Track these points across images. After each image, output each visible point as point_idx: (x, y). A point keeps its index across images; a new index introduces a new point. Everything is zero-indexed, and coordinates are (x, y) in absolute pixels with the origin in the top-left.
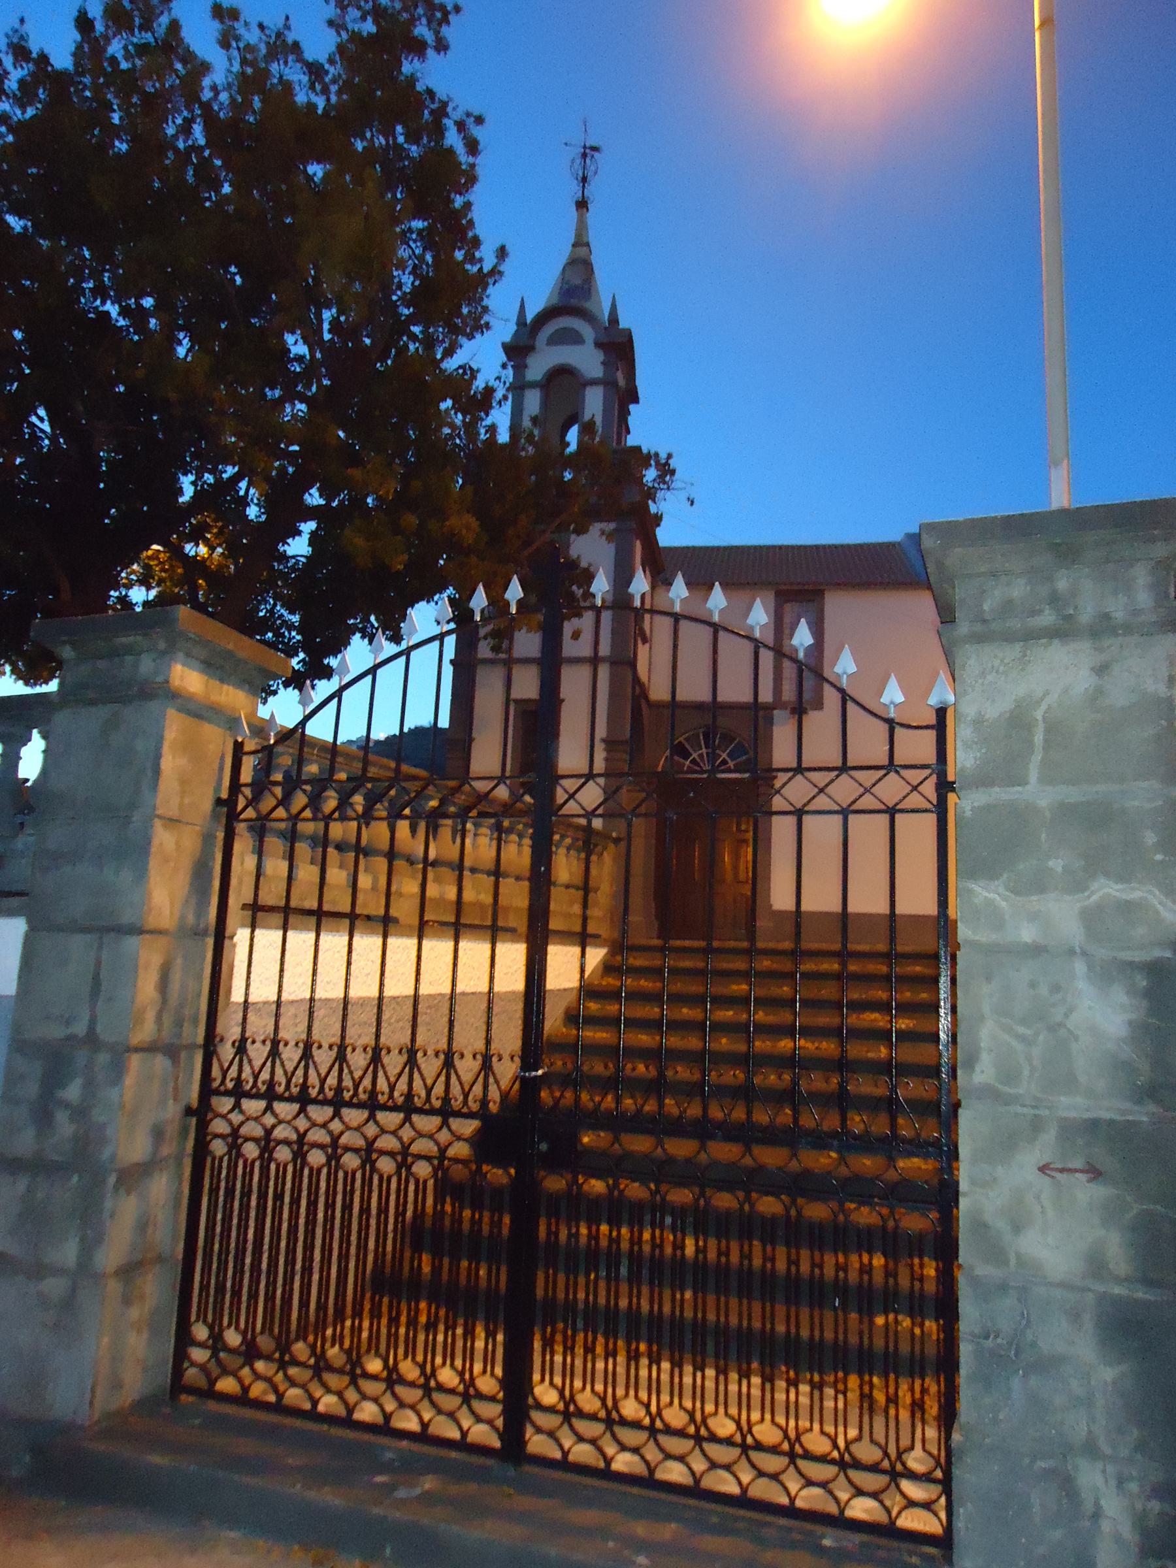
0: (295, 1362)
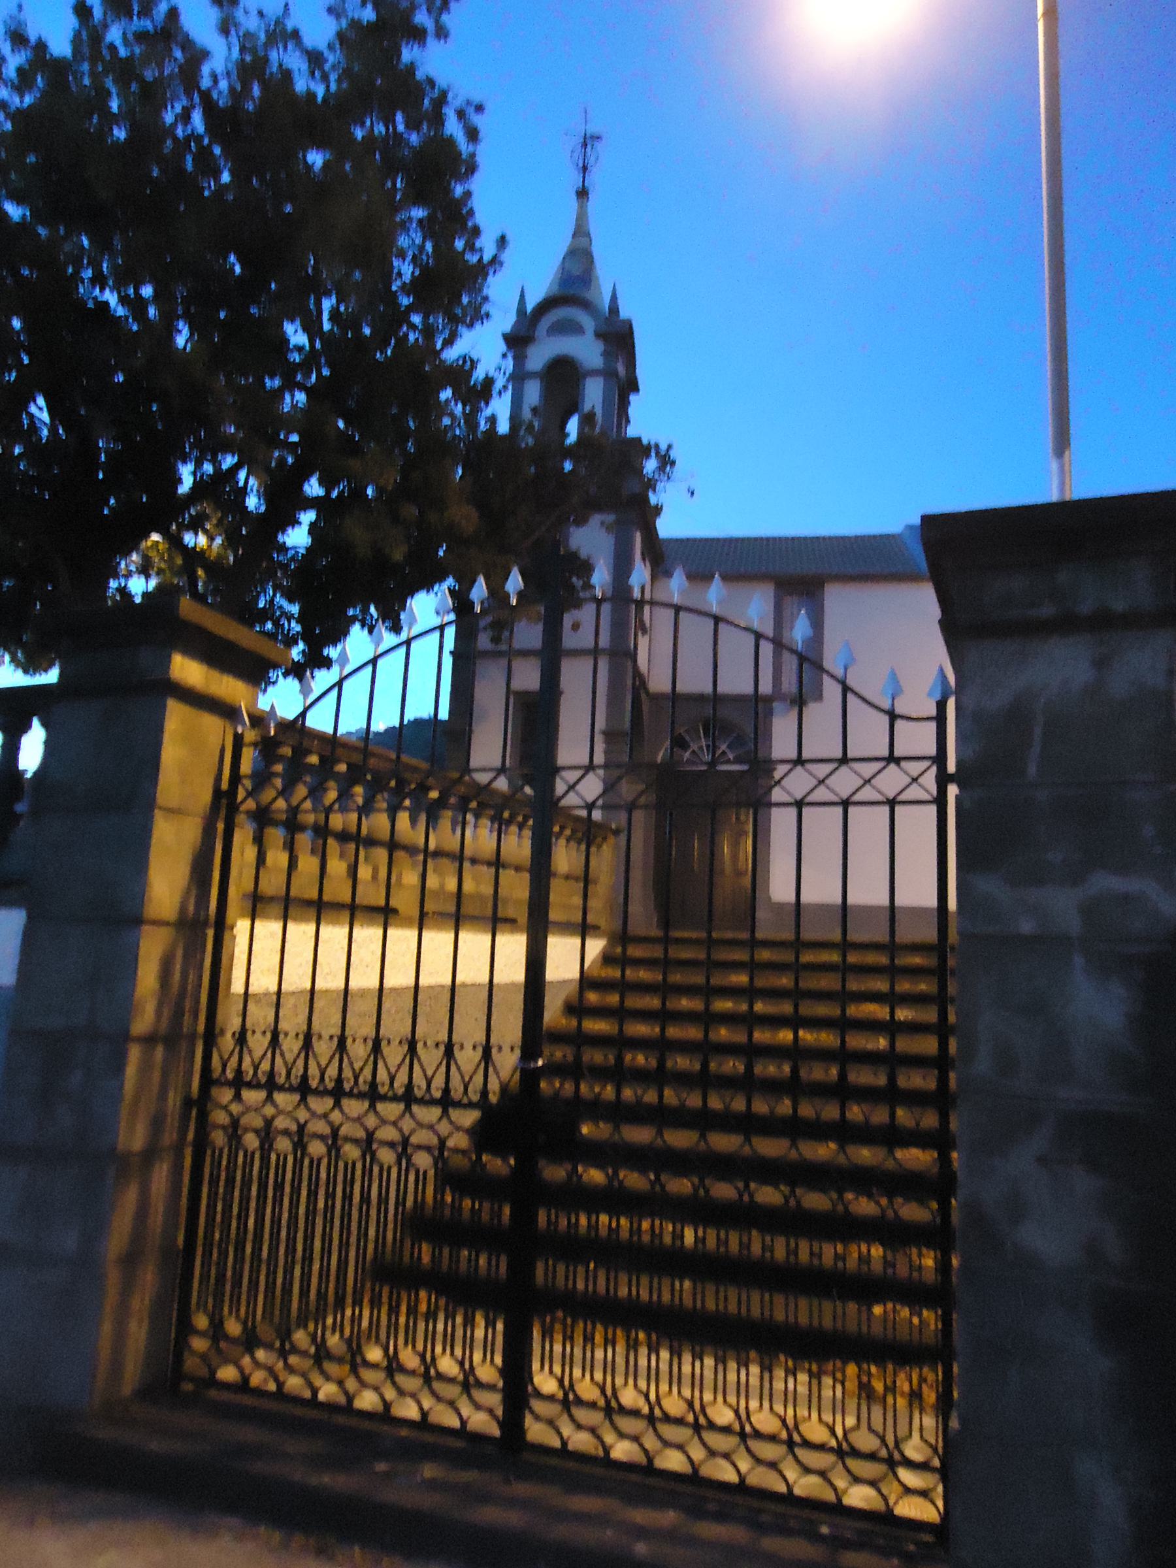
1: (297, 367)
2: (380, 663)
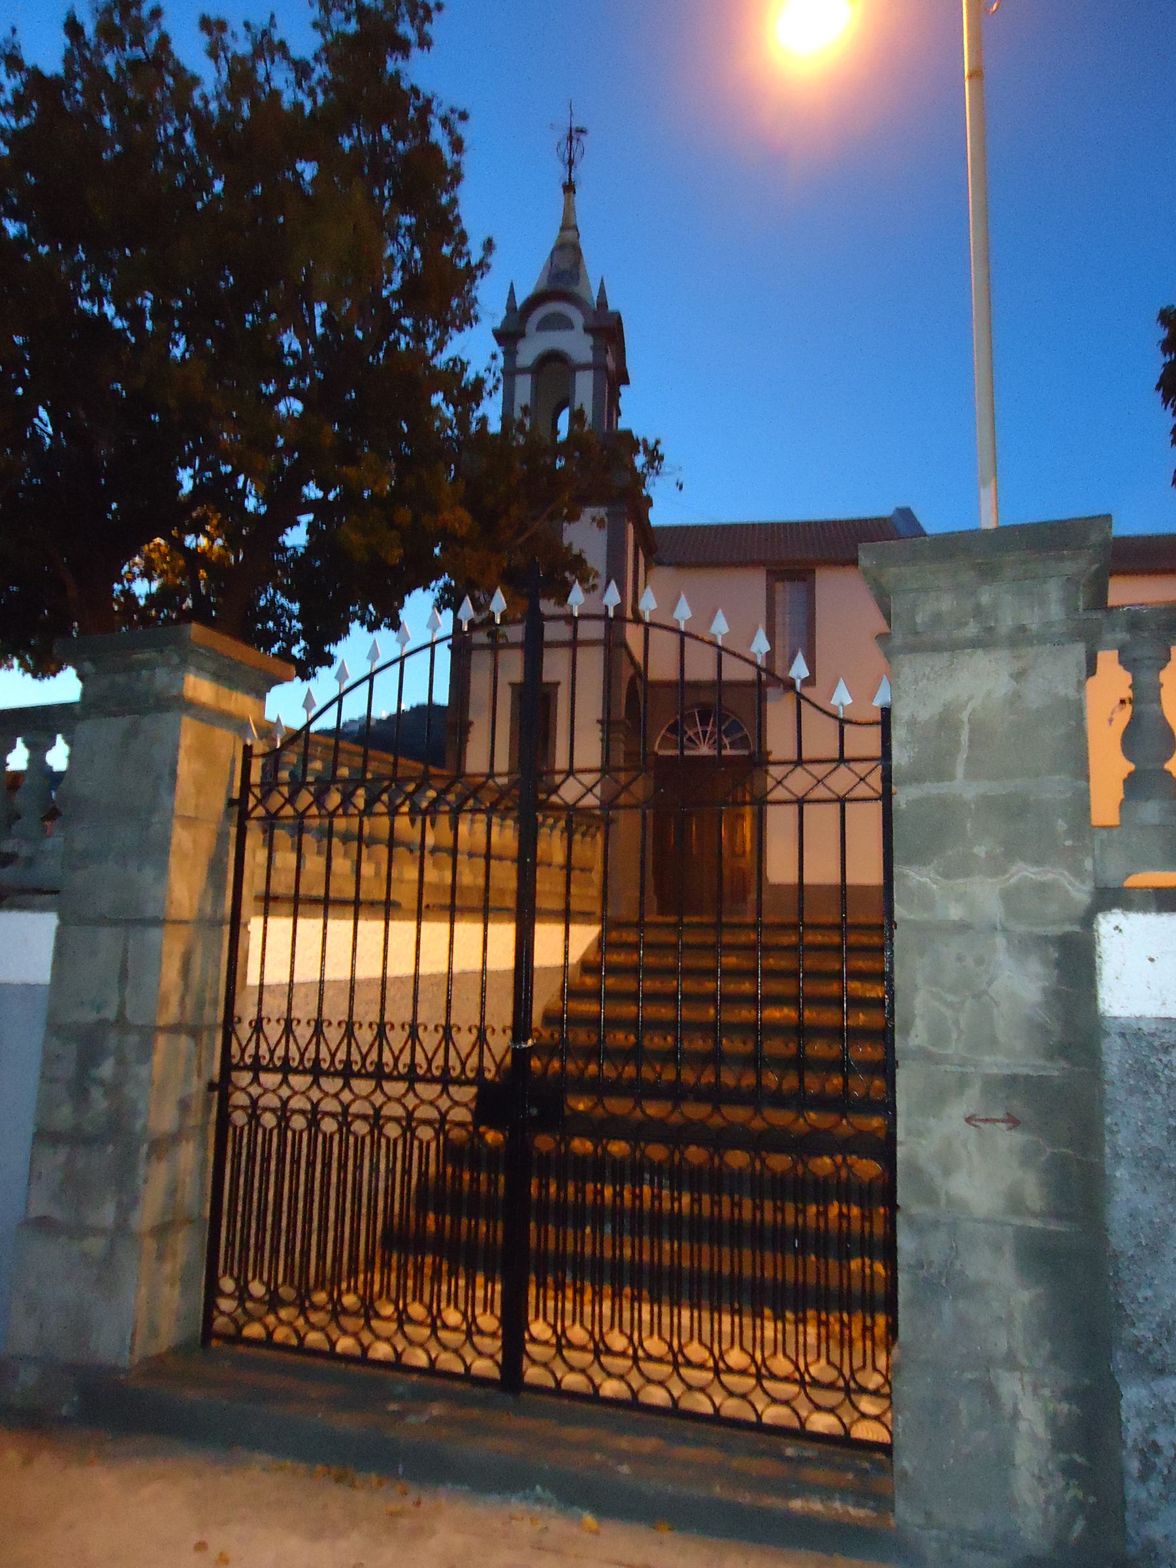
0: (316, 1308)
2: (377, 678)
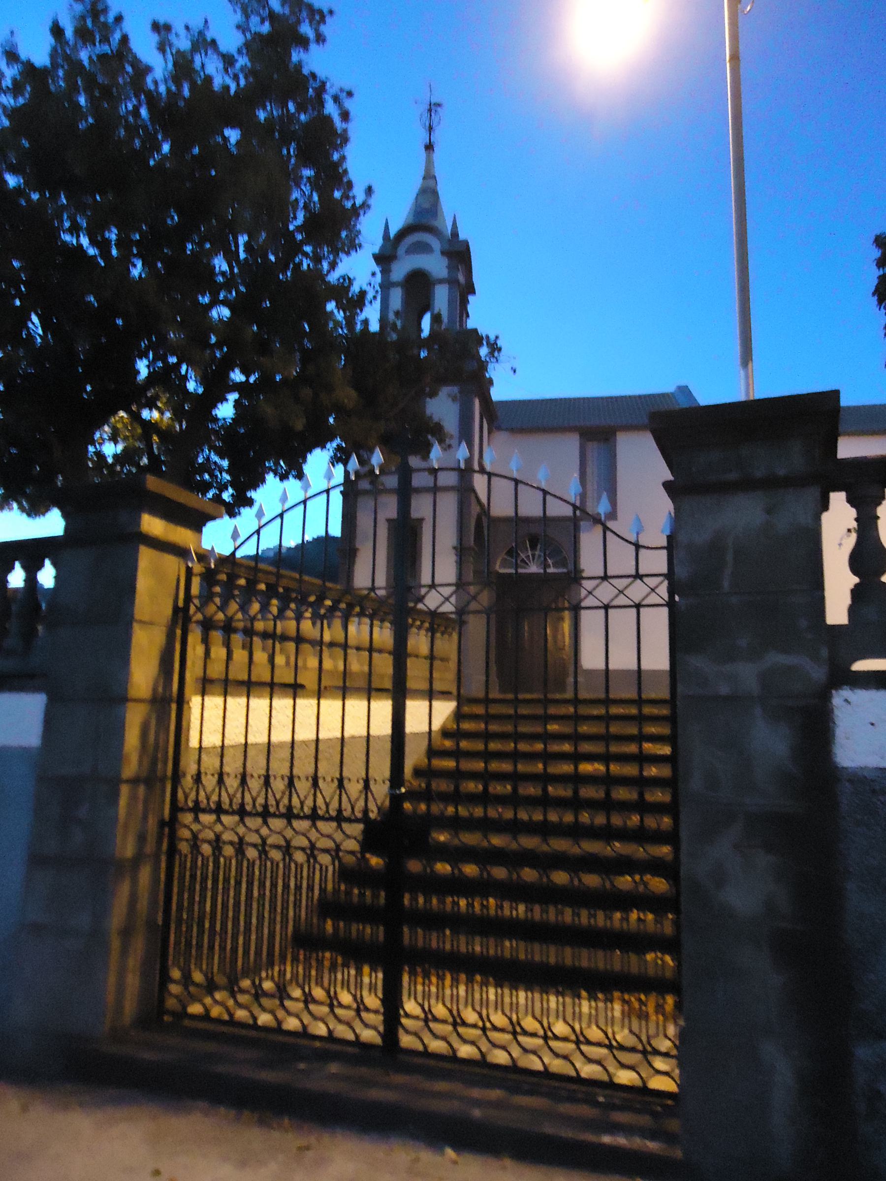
1: (221, 286)
